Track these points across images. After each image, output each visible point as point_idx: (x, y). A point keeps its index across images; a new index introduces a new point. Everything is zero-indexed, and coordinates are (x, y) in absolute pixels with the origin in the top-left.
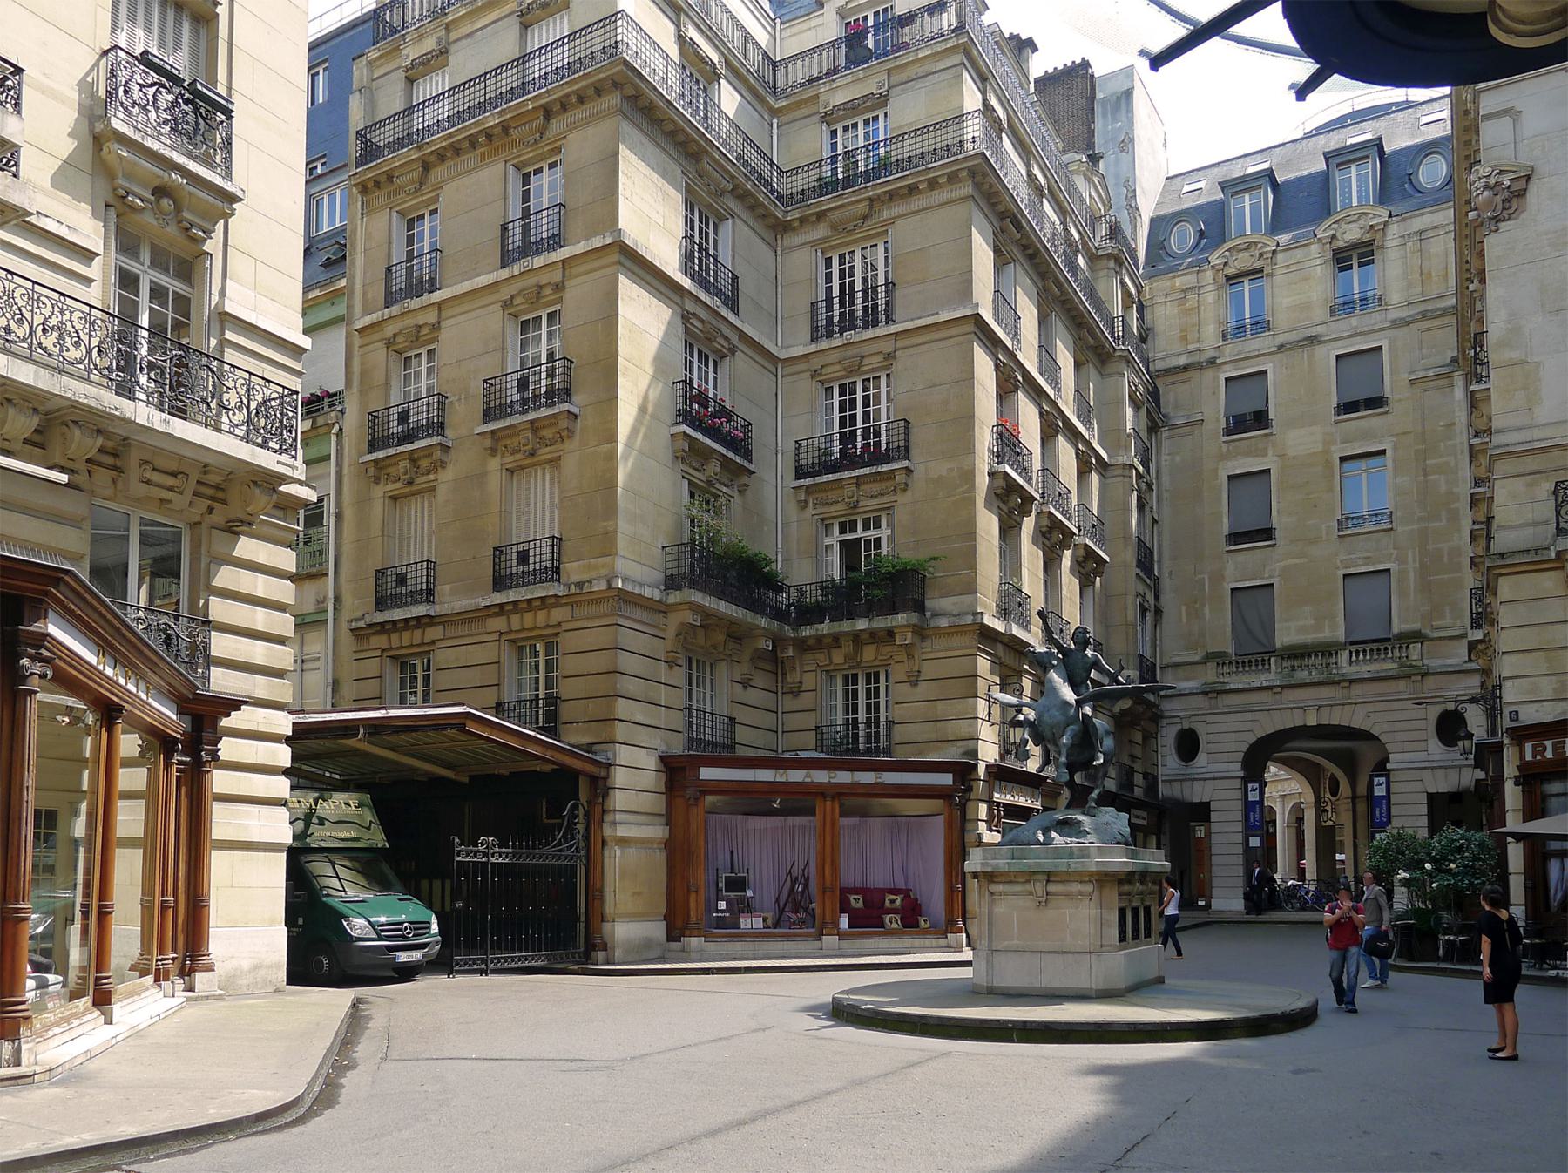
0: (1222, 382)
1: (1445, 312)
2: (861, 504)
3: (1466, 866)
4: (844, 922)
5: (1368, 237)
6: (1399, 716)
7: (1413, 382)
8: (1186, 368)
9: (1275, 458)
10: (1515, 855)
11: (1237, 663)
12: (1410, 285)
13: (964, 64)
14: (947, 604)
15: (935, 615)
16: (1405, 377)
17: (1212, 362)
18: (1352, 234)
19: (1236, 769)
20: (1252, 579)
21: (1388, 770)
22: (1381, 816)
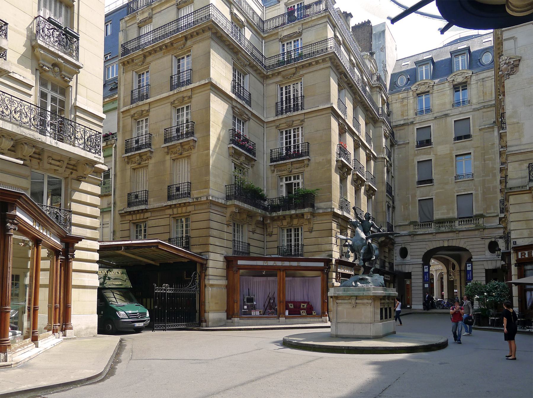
0: (416, 130)
1: (491, 106)
2: (293, 171)
3: (498, 294)
4: (287, 313)
5: (465, 80)
6: (475, 243)
7: (480, 130)
8: (403, 125)
9: (434, 156)
10: (515, 290)
11: (421, 225)
12: (479, 97)
13: (328, 22)
14: (322, 205)
15: (318, 209)
16: (478, 128)
17: (412, 123)
18: (460, 79)
19: (420, 261)
20: (426, 197)
21: (472, 261)
22: (469, 277)
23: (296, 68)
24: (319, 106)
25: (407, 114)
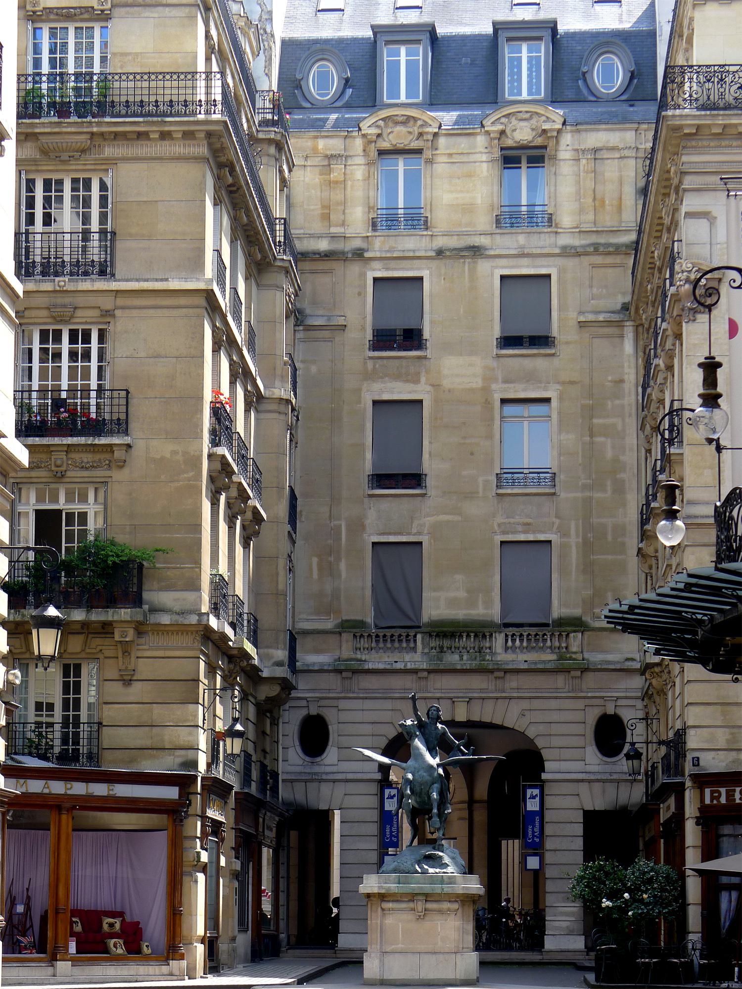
0: (370, 282)
1: (618, 250)
2: (69, 474)
3: (655, 896)
4: (72, 947)
5: (539, 141)
6: (555, 717)
7: (582, 325)
8: (327, 256)
9: (429, 388)
10: (694, 888)
11: (377, 636)
12: (581, 211)
13: (199, 6)
14: (166, 598)
15: (154, 610)
16: (573, 316)
17: (359, 254)
18: (522, 133)
21: (544, 781)
22: (534, 836)
23: (92, 134)
25: (342, 217)
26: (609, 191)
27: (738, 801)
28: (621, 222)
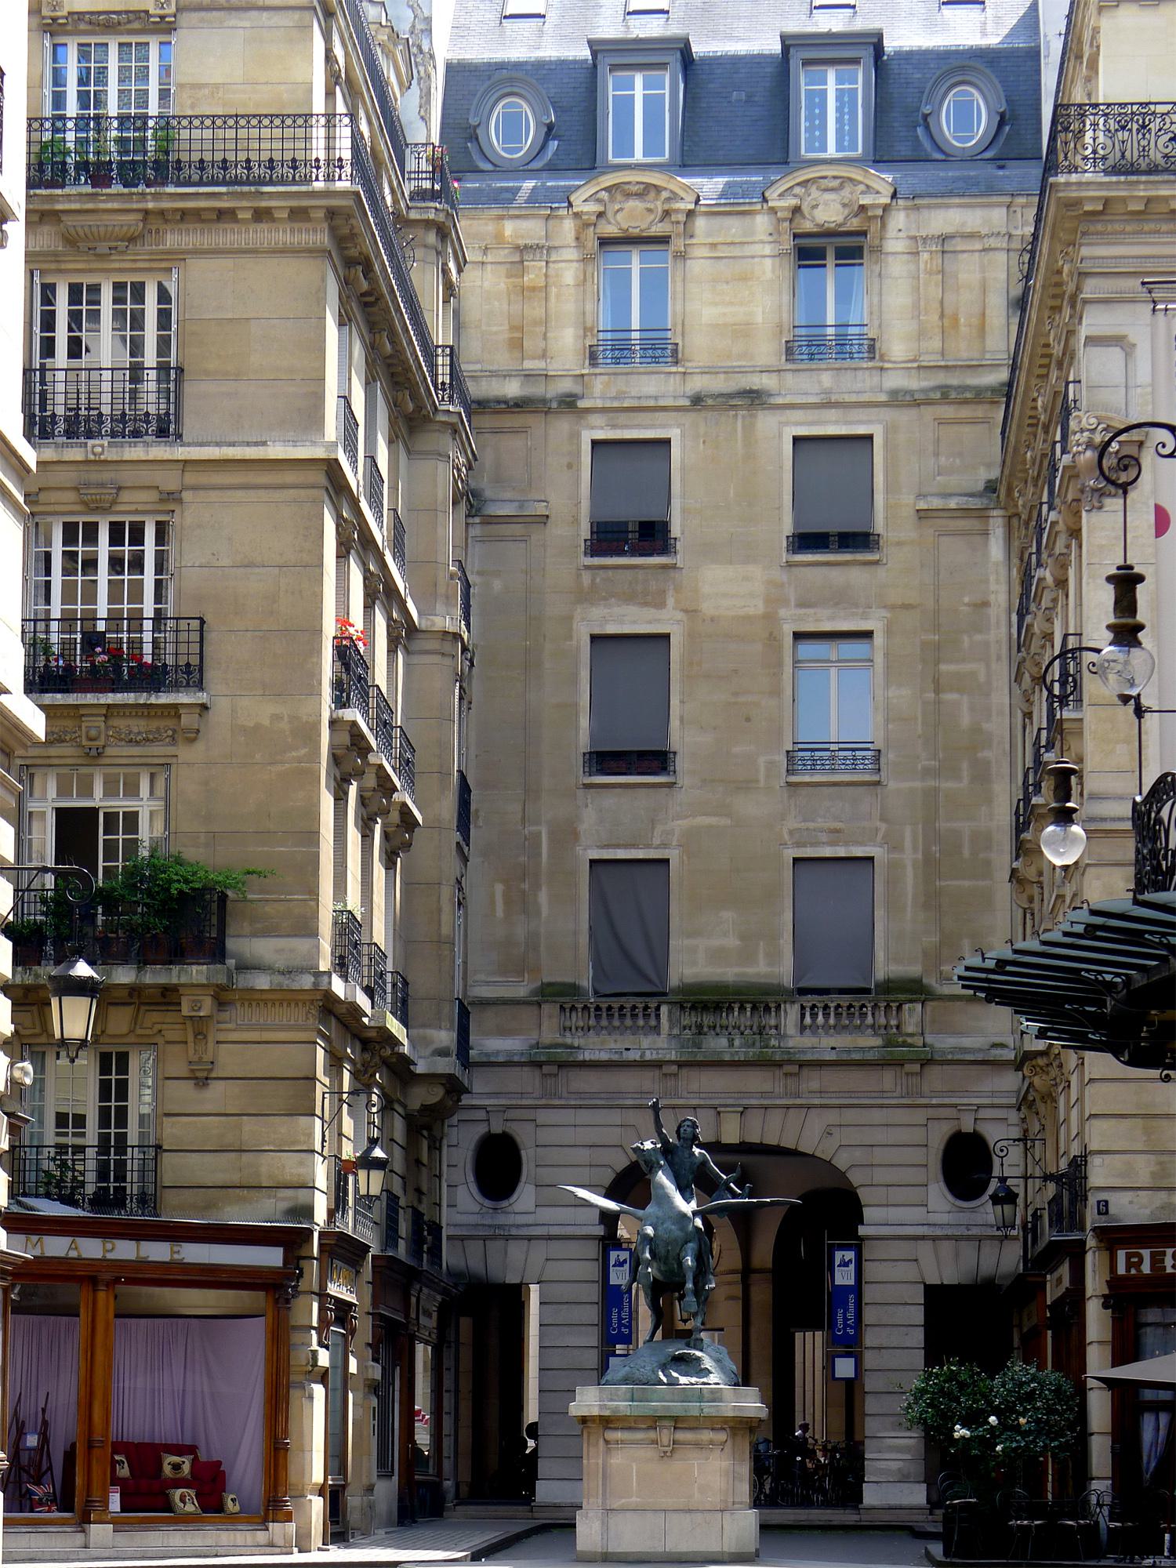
0: (586, 448)
1: (979, 396)
2: (109, 751)
3: (1038, 1421)
4: (115, 1502)
5: (854, 224)
6: (879, 1136)
7: (923, 515)
8: (519, 405)
9: (680, 615)
10: (1099, 1408)
11: (598, 1008)
12: (922, 334)
13: (315, 9)
14: (263, 948)
15: (244, 967)
16: (908, 501)
17: (569, 403)
18: (828, 212)
21: (862, 1239)
22: (846, 1325)
24: (264, 444)
25: (542, 344)
26: (965, 303)
27: (1169, 1270)
28: (984, 351)
